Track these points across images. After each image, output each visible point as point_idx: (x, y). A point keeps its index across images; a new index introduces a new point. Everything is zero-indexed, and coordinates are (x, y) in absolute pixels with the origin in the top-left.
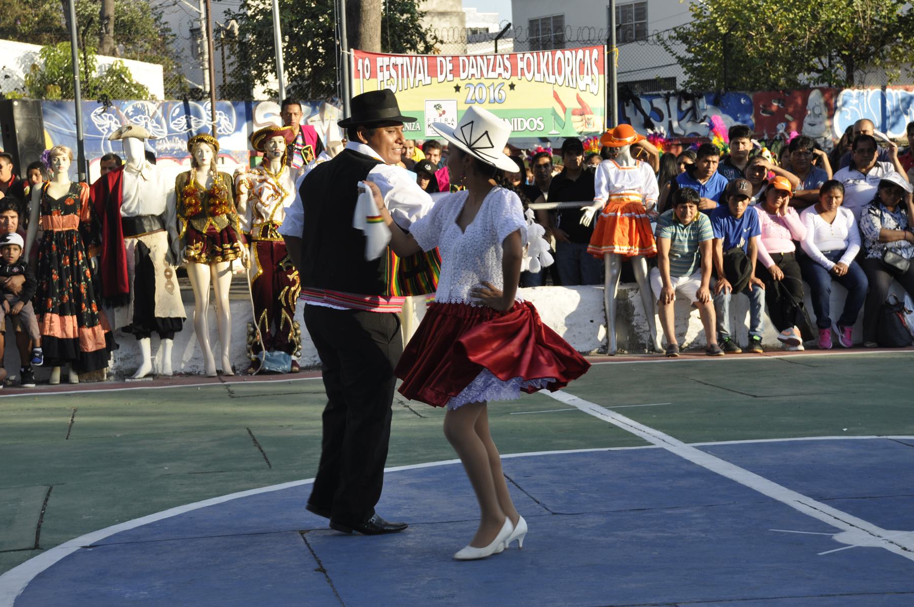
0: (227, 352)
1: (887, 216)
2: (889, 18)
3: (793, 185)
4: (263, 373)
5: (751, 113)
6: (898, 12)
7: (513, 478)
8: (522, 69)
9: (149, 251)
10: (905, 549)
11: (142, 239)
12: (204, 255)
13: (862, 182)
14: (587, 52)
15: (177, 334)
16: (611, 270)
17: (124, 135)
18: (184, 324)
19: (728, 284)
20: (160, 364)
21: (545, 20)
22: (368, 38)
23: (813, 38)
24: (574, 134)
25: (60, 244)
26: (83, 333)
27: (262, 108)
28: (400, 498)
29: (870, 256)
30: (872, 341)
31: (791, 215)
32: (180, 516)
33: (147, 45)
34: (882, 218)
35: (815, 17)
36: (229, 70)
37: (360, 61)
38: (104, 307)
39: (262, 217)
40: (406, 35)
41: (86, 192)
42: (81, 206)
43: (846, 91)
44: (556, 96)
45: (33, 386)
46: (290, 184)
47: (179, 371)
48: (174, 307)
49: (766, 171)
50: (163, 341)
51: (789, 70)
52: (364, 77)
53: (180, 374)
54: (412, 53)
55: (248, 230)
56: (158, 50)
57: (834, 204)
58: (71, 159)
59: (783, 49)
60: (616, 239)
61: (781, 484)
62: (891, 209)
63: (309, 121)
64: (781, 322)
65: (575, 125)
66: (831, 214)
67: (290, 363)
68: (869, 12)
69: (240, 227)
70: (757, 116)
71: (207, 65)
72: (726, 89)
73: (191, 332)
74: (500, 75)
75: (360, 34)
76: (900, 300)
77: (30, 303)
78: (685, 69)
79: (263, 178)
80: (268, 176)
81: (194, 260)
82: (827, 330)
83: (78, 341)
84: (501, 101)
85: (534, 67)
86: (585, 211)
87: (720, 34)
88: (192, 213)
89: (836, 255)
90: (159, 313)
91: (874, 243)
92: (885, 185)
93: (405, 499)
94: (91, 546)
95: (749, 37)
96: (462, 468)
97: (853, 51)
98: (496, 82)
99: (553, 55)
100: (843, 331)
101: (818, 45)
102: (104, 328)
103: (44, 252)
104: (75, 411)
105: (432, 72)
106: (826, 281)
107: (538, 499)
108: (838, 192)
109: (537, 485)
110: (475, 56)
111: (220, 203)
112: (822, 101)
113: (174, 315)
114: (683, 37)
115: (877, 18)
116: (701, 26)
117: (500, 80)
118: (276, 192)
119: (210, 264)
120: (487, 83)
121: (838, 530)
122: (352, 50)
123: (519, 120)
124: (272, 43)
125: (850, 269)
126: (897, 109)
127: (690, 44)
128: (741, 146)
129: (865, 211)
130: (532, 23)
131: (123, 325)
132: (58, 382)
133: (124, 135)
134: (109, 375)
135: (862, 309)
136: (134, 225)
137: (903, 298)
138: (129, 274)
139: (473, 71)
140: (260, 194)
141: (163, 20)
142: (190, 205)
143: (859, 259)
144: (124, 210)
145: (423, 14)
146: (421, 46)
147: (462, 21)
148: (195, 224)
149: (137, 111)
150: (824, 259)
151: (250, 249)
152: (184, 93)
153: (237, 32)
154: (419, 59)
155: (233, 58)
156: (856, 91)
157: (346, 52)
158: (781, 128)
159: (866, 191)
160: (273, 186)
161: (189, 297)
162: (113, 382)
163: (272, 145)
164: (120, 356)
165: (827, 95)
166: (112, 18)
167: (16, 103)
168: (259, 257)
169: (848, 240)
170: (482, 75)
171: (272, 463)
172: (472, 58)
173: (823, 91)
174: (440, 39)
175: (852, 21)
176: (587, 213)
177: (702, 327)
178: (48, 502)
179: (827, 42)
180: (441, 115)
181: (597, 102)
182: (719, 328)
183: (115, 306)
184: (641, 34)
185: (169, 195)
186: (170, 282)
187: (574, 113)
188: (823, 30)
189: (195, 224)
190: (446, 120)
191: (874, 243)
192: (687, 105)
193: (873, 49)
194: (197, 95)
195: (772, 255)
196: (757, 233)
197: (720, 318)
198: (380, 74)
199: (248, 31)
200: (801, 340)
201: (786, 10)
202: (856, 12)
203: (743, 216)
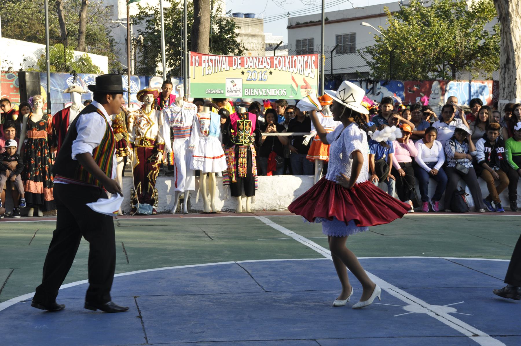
1: (458, 146)
2: (474, 46)
3: (412, 128)
4: (138, 214)
5: (403, 91)
6: (478, 44)
10: (437, 315)
13: (446, 128)
14: (310, 57)
16: (318, 168)
17: (71, 91)
19: (377, 177)
21: (304, 41)
22: (202, 45)
23: (435, 55)
25: (36, 145)
27: (153, 80)
28: (190, 281)
29: (449, 166)
30: (449, 209)
31: (410, 144)
32: (75, 287)
33: (102, 46)
34: (456, 147)
35: (437, 44)
36: (138, 60)
37: (194, 57)
39: (140, 135)
40: (229, 45)
41: (51, 119)
43: (451, 82)
44: (293, 79)
45: (19, 217)
49: (398, 121)
52: (195, 65)
54: (231, 54)
58: (43, 102)
60: (321, 152)
61: (384, 280)
63: (178, 87)
66: (430, 144)
67: (152, 210)
68: (463, 43)
69: (129, 140)
70: (406, 93)
72: (391, 79)
74: (265, 67)
75: (198, 44)
77: (20, 175)
78: (370, 68)
79: (141, 115)
82: (426, 202)
83: (43, 195)
84: (265, 80)
85: (282, 63)
86: (305, 137)
89: (432, 165)
93: (193, 281)
94: (25, 301)
95: (403, 53)
97: (455, 62)
98: (263, 70)
99: (292, 58)
100: (434, 203)
101: (438, 58)
103: (27, 149)
104: (37, 231)
105: (230, 64)
106: (426, 177)
107: (260, 284)
108: (434, 133)
109: (262, 276)
110: (252, 57)
111: (119, 127)
112: (439, 87)
114: (370, 51)
115: (468, 46)
116: (380, 46)
117: (265, 69)
118: (148, 122)
120: (258, 71)
125: (439, 172)
126: (477, 92)
127: (374, 55)
130: (298, 41)
132: (32, 216)
133: (71, 91)
135: (444, 193)
137: (465, 187)
139: (251, 64)
140: (140, 123)
141: (111, 34)
146: (236, 51)
147: (263, 39)
150: (426, 166)
151: (133, 151)
153: (142, 41)
154: (224, 58)
155: (141, 54)
156: (456, 82)
157: (186, 52)
165: (441, 84)
166: (84, 32)
167: (27, 74)
168: (138, 155)
169: (439, 157)
170: (256, 67)
171: (130, 260)
172: (251, 58)
173: (440, 82)
174: (246, 48)
175: (455, 47)
176: (306, 139)
178: (10, 278)
179: (442, 57)
181: (314, 83)
184: (352, 50)
187: (302, 87)
188: (441, 51)
192: (370, 86)
193: (466, 62)
195: (400, 164)
196: (392, 152)
198: (203, 64)
199: (148, 40)
201: (422, 40)
202: (457, 43)
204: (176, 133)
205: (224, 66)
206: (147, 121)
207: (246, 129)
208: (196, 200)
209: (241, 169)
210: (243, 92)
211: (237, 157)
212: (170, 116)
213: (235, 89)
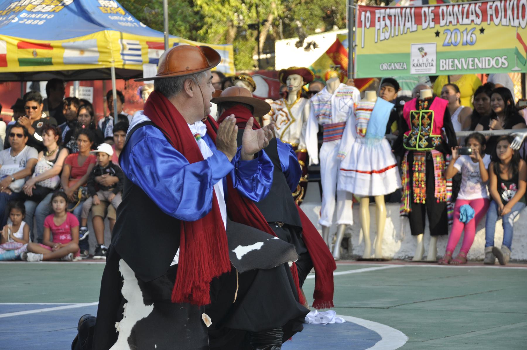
37: (363, 13)
44: (519, 38)
52: (365, 26)
74: (473, 21)
84: (472, 43)
98: (469, 28)
117: (473, 26)
120: (462, 28)
160: (286, 113)
170: (458, 22)
180: (423, 56)
190: (427, 60)
198: (377, 24)
204: (325, 134)
205: (408, 25)
206: (287, 116)
207: (422, 124)
208: (358, 239)
209: (417, 191)
210: (438, 66)
211: (411, 172)
212: (316, 107)
213: (425, 61)
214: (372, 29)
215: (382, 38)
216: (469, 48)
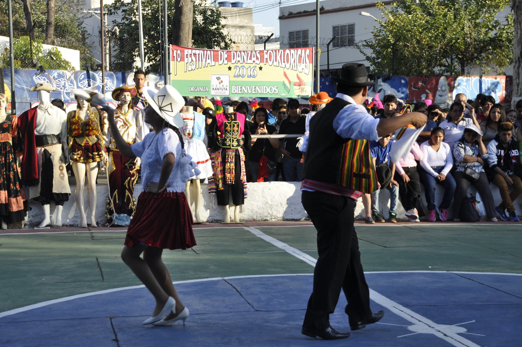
0: (94, 213)
1: (468, 148)
4: (114, 226)
7: (239, 289)
8: (267, 59)
9: (51, 155)
10: (445, 335)
11: (47, 148)
12: (82, 158)
13: (455, 129)
14: (303, 50)
15: (65, 203)
17: (38, 89)
18: (70, 197)
20: (55, 219)
21: (298, 32)
22: (184, 38)
24: (294, 96)
26: (10, 200)
29: (458, 170)
33: (73, 39)
34: (465, 149)
35: (444, 36)
37: (175, 51)
38: (24, 186)
41: (15, 120)
42: (12, 128)
43: (460, 78)
46: (133, 119)
47: (66, 224)
48: (64, 187)
50: (57, 206)
51: (429, 65)
52: (177, 60)
53: (67, 226)
54: (217, 48)
55: (108, 145)
56: (81, 42)
57: (439, 141)
58: (7, 102)
59: (425, 53)
61: (387, 297)
62: (470, 144)
64: (407, 205)
65: (296, 91)
66: (437, 146)
69: (103, 143)
71: (108, 51)
72: (393, 75)
73: (74, 202)
74: (254, 61)
76: (473, 195)
80: (120, 115)
81: (76, 161)
82: (433, 211)
84: (254, 77)
85: (273, 58)
86: (299, 140)
87: (391, 44)
88: (76, 134)
89: (439, 169)
90: (55, 190)
91: (460, 163)
92: (468, 131)
96: (364, 267)
98: (252, 66)
99: (284, 51)
100: (442, 212)
101: (445, 51)
102: (23, 198)
105: (216, 59)
107: (250, 302)
109: (252, 294)
110: (240, 52)
111: (92, 129)
112: (446, 83)
113: (64, 192)
117: (254, 65)
118: (125, 123)
119: (86, 163)
120: (247, 66)
121: (411, 324)
122: (171, 45)
123: (264, 87)
124: (138, 39)
125: (447, 177)
128: (391, 107)
129: (456, 145)
130: (291, 33)
131: (34, 197)
133: (38, 89)
134: (25, 225)
135: (453, 200)
136: (42, 140)
137: (475, 194)
138: (39, 168)
139: (239, 59)
141: (83, 26)
142: (75, 129)
143: (452, 171)
144: (37, 131)
145: (223, 27)
146: (223, 44)
147: (253, 31)
148: (78, 140)
149: (60, 76)
150: (432, 171)
151: (109, 155)
152: (89, 66)
153: (118, 33)
154: (209, 52)
156: (466, 78)
157: (167, 46)
158: (423, 97)
159: (457, 134)
160: (123, 120)
161: (73, 181)
162: (27, 229)
163: (123, 97)
164: (33, 214)
166: (53, 24)
169: (446, 161)
170: (244, 61)
171: (105, 277)
173: (447, 77)
177: (363, 207)
179: (450, 50)
180: (220, 83)
181: (308, 79)
182: (373, 208)
183: (30, 186)
184: (351, 42)
185: (63, 124)
186: (62, 173)
189: (78, 140)
190: (223, 86)
191: (460, 163)
193: (476, 55)
194: (100, 67)
195: (404, 168)
197: (373, 202)
198: (186, 59)
200: (418, 216)
202: (466, 34)
203: (387, 146)
206: (124, 122)
209: (228, 175)
211: (224, 162)
213: (221, 87)
214: (182, 62)
215: (190, 69)
216: (251, 79)
